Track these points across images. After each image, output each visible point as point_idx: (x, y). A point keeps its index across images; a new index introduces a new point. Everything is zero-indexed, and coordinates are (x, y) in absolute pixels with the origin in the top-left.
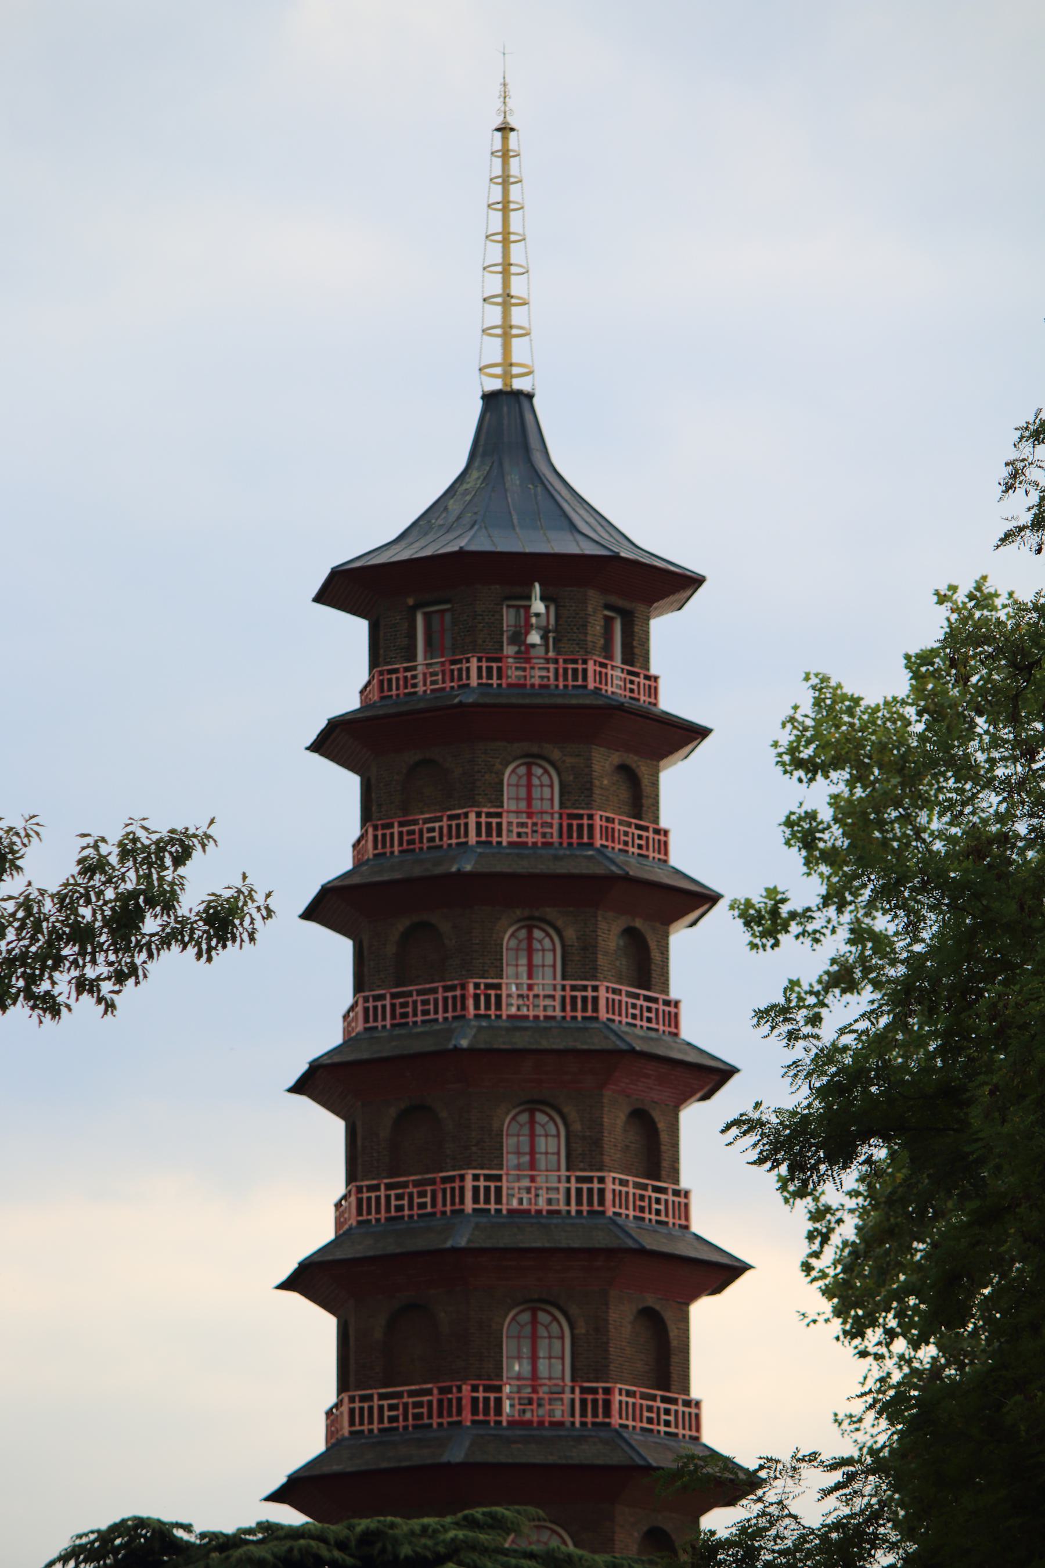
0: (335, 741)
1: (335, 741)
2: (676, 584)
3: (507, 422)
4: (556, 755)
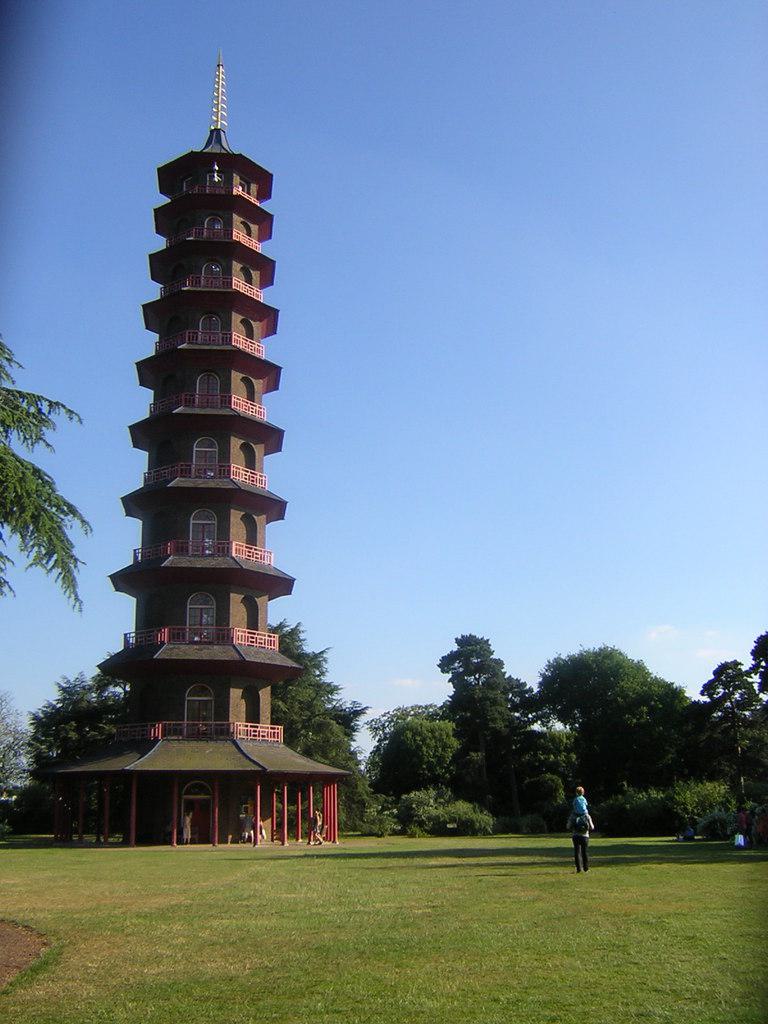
2: (263, 181)
3: (215, 135)
4: (220, 213)
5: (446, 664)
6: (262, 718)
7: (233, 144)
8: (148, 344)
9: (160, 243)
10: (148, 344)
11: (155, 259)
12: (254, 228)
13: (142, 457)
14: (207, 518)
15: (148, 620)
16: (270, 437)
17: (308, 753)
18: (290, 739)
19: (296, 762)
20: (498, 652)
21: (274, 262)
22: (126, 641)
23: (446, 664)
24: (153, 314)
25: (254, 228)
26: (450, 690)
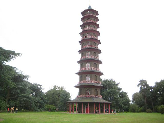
0: (79, 62)
1: (79, 62)
2: (97, 13)
6: (98, 94)
7: (93, 8)
10: (81, 30)
13: (78, 77)
16: (99, 52)
25: (95, 20)
26: (139, 90)
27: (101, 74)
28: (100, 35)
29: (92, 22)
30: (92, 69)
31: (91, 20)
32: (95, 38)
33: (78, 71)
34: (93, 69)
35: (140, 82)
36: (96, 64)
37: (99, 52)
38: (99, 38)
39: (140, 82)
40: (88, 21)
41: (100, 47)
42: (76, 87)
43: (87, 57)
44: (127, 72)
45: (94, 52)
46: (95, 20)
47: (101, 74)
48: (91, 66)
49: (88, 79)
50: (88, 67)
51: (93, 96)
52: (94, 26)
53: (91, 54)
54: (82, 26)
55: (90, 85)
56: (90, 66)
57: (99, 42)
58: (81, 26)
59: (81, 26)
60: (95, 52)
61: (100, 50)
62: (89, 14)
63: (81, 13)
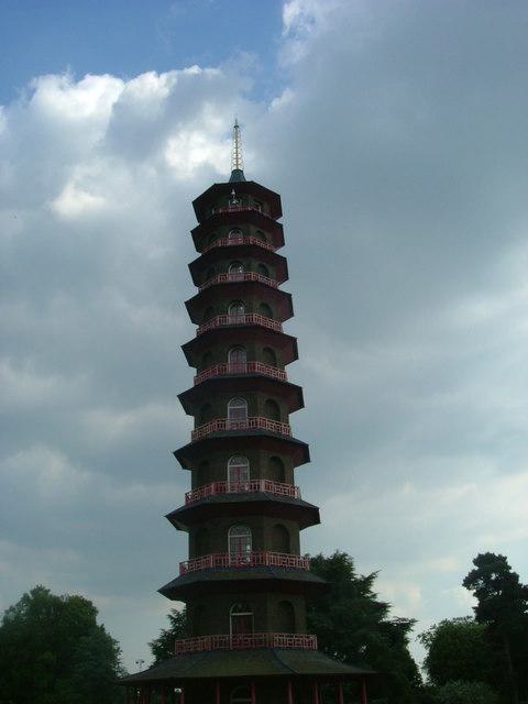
0: (177, 518)
1: (177, 518)
4: (240, 226)
5: (469, 582)
8: (183, 427)
9: (194, 291)
10: (187, 377)
11: (188, 349)
12: (268, 235)
13: (183, 538)
14: (241, 404)
15: (197, 549)
16: (301, 453)
17: (347, 662)
18: (326, 645)
19: (333, 665)
20: (509, 562)
21: (296, 357)
22: (187, 497)
23: (469, 582)
24: (193, 306)
25: (268, 235)
26: (475, 602)
27: (311, 516)
28: (301, 405)
29: (263, 328)
30: (263, 489)
31: (247, 233)
32: (271, 324)
33: (172, 575)
34: (267, 487)
35: (476, 562)
36: (278, 410)
37: (301, 453)
38: (293, 373)
39: (476, 562)
40: (230, 321)
41: (299, 425)
42: (170, 592)
43: (228, 422)
44: (420, 538)
45: (278, 525)
46: (271, 270)
47: (311, 516)
48: (255, 475)
49: (241, 547)
50: (236, 416)
51: (279, 638)
52: (274, 459)
53: (253, 411)
54: (194, 352)
55: (253, 575)
56: (248, 471)
57: (294, 397)
58: (185, 347)
59: (185, 347)
60: (275, 398)
61: (298, 390)
62: (235, 205)
63: (191, 266)
